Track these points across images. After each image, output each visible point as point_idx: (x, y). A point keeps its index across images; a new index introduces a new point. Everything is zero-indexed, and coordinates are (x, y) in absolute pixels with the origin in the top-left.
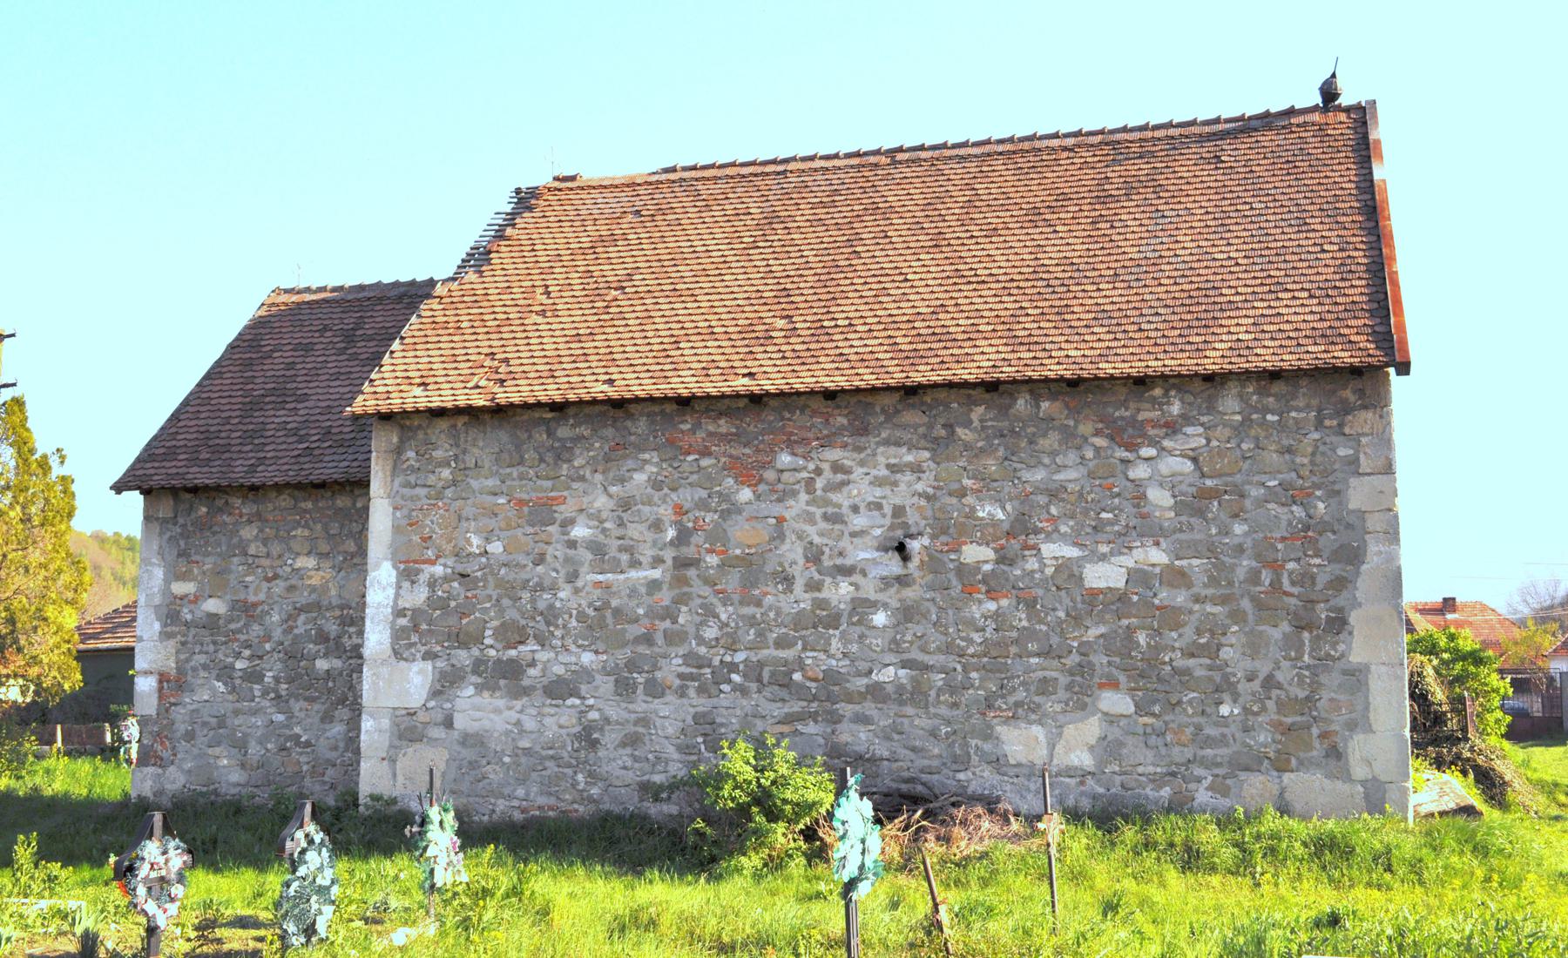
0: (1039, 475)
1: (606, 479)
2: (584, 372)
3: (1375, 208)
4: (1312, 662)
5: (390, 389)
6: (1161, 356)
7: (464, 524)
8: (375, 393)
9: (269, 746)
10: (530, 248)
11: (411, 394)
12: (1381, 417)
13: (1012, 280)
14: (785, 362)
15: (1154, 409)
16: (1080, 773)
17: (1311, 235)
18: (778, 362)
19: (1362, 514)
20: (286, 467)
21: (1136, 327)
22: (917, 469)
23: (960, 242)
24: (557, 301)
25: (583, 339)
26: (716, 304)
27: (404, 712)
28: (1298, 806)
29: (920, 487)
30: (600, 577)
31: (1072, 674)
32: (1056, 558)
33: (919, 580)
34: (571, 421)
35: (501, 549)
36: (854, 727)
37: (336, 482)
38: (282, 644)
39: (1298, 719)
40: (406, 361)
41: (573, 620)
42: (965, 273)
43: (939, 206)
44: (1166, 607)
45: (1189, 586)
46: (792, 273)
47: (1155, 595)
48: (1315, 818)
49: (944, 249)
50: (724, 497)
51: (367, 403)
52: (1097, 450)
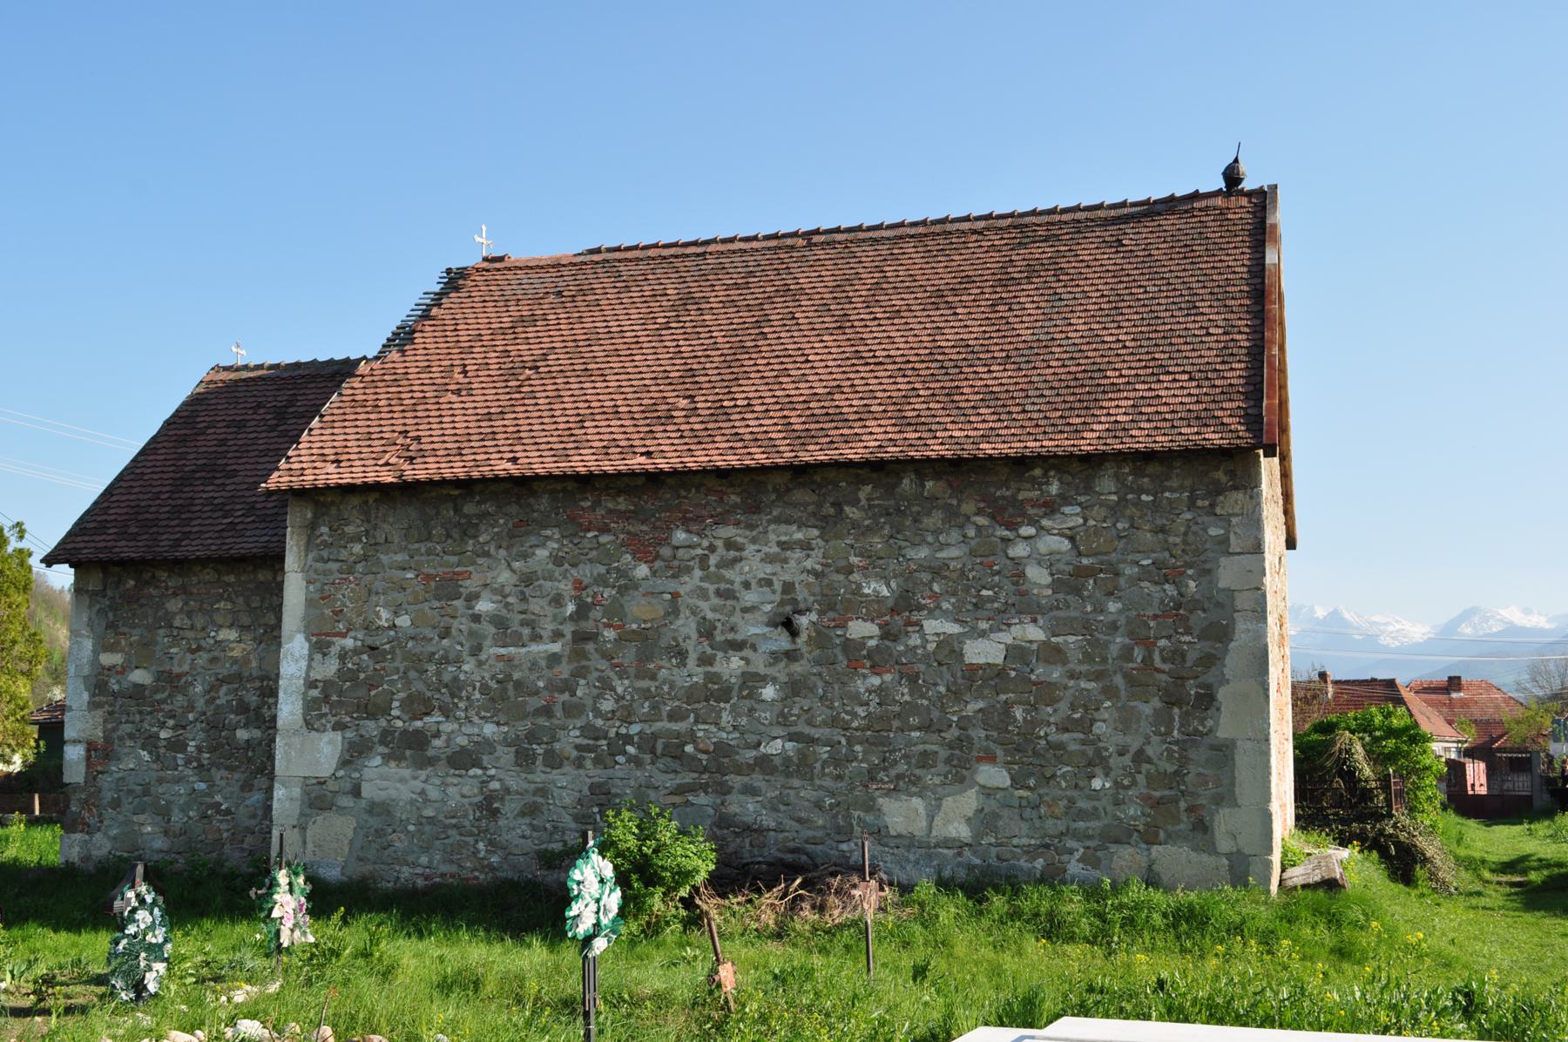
0: (922, 553)
1: (509, 555)
2: (491, 450)
3: (1263, 291)
4: (1181, 737)
5: (305, 465)
6: (1040, 437)
7: (374, 598)
8: (290, 469)
9: (191, 813)
10: (452, 328)
11: (324, 471)
12: (1251, 497)
13: (909, 362)
14: (683, 441)
15: (1035, 490)
16: (958, 844)
17: (1198, 318)
18: (676, 441)
19: (1230, 593)
20: (210, 541)
21: (1020, 409)
22: (806, 546)
23: (863, 323)
24: (473, 380)
25: (494, 417)
26: (624, 383)
27: (314, 781)
28: (1165, 878)
29: (809, 564)
30: (503, 651)
31: (951, 748)
32: (938, 635)
33: (807, 655)
34: (478, 498)
35: (409, 623)
36: (742, 798)
37: (254, 556)
38: (204, 714)
39: (1167, 792)
40: (323, 438)
41: (477, 692)
42: (865, 355)
43: (848, 288)
44: (1042, 683)
45: (1065, 662)
46: (700, 354)
47: (1032, 671)
48: (1179, 891)
49: (847, 331)
50: (622, 573)
51: (281, 480)
52: (979, 528)
